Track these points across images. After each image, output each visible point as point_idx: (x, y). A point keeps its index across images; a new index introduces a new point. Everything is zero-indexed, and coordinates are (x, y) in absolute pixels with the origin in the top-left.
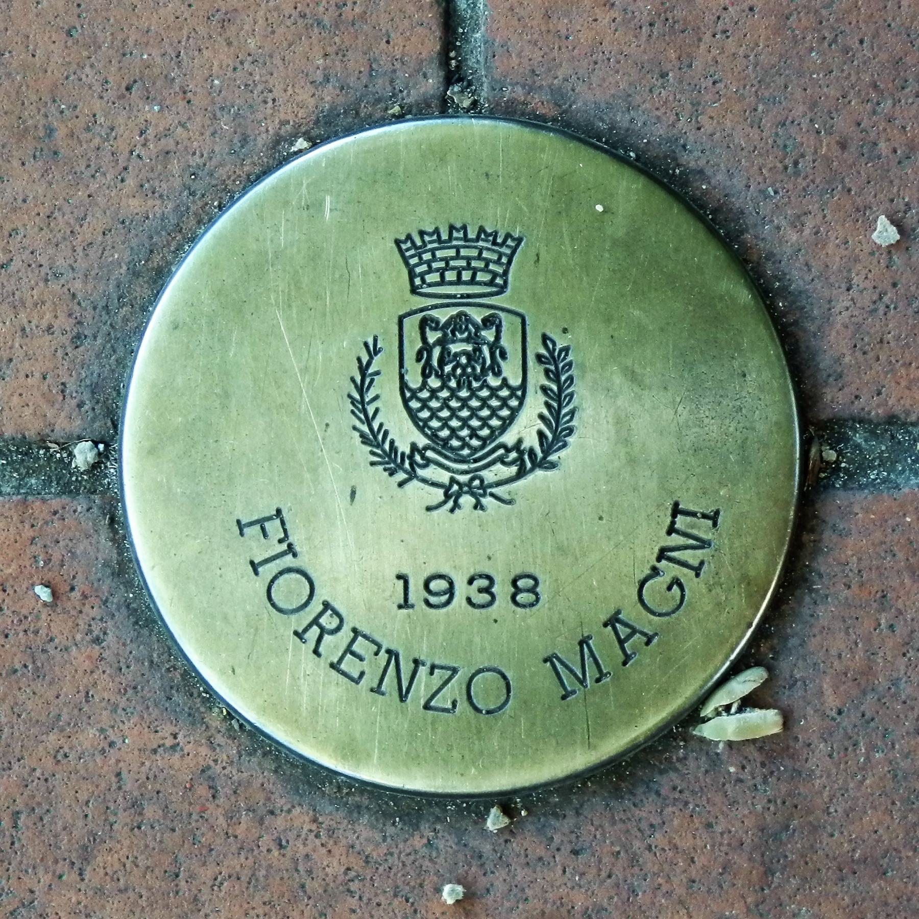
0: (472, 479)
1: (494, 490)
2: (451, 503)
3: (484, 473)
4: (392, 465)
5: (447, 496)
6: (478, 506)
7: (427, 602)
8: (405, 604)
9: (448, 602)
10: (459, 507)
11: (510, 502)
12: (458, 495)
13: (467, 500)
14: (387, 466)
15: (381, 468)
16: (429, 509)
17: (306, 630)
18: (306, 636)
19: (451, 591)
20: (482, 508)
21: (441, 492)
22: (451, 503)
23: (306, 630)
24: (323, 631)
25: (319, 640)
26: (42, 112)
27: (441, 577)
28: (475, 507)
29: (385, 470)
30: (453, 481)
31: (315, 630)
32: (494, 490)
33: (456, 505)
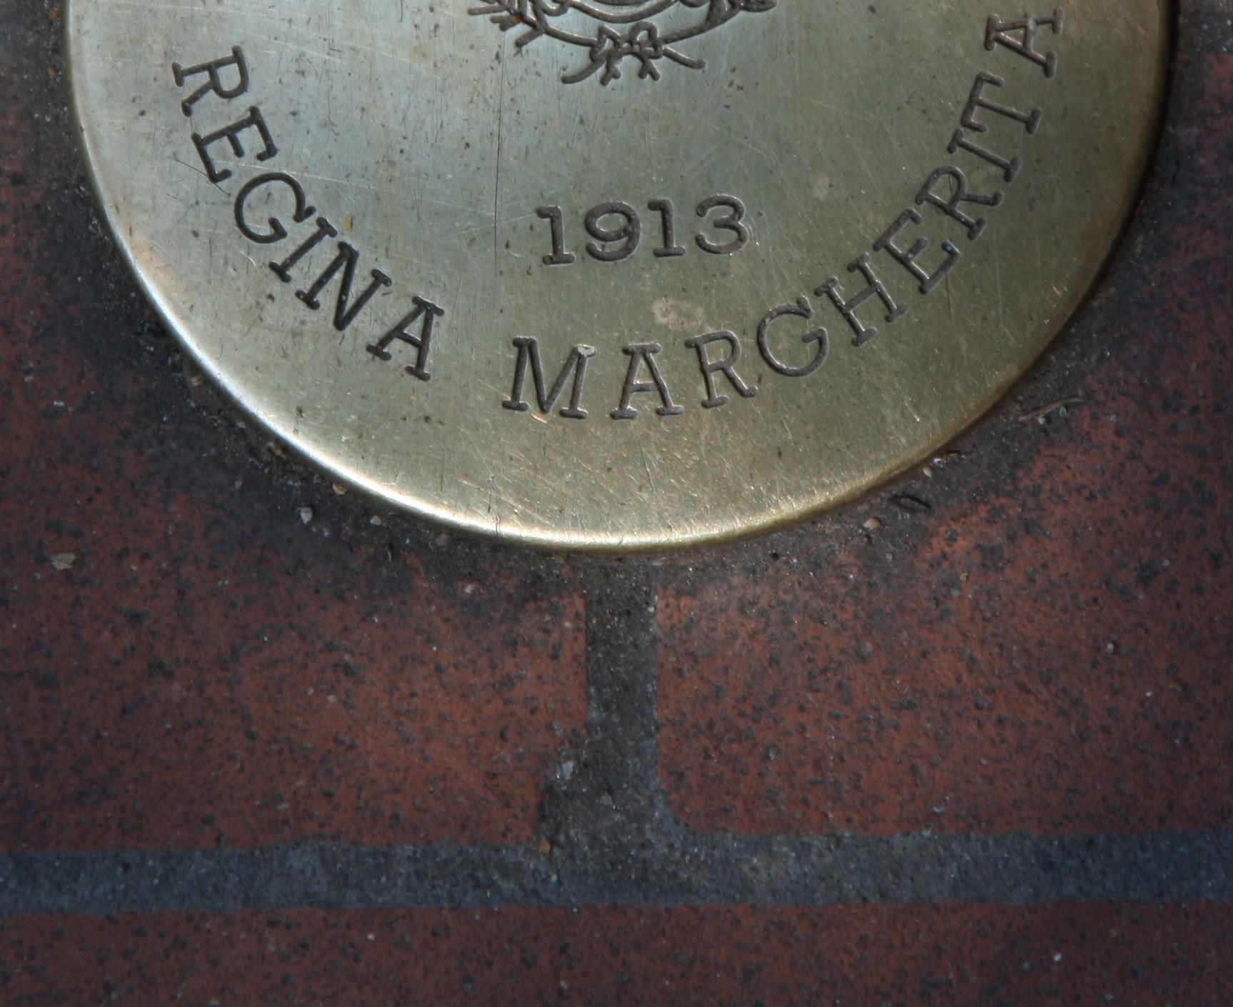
0: (635, 30)
1: (669, 47)
2: (601, 70)
3: (653, 20)
4: (505, 13)
5: (594, 60)
6: (645, 70)
7: (591, 251)
8: (556, 257)
9: (627, 250)
10: (616, 76)
11: (699, 65)
12: (611, 58)
13: (627, 64)
14: (498, 14)
15: (488, 16)
16: (565, 80)
17: (192, 71)
18: (188, 79)
19: (629, 233)
20: (654, 76)
21: (585, 50)
22: (601, 70)
23: (192, 71)
24: (214, 85)
25: (202, 91)
26: (1122, 383)
27: (612, 210)
28: (641, 75)
29: (493, 20)
30: (601, 31)
31: (204, 77)
32: (669, 47)
33: (610, 74)
